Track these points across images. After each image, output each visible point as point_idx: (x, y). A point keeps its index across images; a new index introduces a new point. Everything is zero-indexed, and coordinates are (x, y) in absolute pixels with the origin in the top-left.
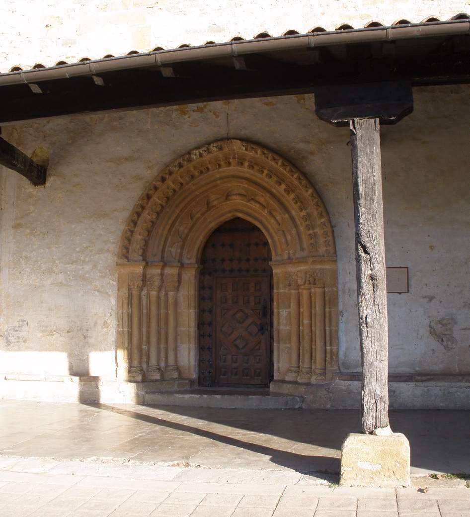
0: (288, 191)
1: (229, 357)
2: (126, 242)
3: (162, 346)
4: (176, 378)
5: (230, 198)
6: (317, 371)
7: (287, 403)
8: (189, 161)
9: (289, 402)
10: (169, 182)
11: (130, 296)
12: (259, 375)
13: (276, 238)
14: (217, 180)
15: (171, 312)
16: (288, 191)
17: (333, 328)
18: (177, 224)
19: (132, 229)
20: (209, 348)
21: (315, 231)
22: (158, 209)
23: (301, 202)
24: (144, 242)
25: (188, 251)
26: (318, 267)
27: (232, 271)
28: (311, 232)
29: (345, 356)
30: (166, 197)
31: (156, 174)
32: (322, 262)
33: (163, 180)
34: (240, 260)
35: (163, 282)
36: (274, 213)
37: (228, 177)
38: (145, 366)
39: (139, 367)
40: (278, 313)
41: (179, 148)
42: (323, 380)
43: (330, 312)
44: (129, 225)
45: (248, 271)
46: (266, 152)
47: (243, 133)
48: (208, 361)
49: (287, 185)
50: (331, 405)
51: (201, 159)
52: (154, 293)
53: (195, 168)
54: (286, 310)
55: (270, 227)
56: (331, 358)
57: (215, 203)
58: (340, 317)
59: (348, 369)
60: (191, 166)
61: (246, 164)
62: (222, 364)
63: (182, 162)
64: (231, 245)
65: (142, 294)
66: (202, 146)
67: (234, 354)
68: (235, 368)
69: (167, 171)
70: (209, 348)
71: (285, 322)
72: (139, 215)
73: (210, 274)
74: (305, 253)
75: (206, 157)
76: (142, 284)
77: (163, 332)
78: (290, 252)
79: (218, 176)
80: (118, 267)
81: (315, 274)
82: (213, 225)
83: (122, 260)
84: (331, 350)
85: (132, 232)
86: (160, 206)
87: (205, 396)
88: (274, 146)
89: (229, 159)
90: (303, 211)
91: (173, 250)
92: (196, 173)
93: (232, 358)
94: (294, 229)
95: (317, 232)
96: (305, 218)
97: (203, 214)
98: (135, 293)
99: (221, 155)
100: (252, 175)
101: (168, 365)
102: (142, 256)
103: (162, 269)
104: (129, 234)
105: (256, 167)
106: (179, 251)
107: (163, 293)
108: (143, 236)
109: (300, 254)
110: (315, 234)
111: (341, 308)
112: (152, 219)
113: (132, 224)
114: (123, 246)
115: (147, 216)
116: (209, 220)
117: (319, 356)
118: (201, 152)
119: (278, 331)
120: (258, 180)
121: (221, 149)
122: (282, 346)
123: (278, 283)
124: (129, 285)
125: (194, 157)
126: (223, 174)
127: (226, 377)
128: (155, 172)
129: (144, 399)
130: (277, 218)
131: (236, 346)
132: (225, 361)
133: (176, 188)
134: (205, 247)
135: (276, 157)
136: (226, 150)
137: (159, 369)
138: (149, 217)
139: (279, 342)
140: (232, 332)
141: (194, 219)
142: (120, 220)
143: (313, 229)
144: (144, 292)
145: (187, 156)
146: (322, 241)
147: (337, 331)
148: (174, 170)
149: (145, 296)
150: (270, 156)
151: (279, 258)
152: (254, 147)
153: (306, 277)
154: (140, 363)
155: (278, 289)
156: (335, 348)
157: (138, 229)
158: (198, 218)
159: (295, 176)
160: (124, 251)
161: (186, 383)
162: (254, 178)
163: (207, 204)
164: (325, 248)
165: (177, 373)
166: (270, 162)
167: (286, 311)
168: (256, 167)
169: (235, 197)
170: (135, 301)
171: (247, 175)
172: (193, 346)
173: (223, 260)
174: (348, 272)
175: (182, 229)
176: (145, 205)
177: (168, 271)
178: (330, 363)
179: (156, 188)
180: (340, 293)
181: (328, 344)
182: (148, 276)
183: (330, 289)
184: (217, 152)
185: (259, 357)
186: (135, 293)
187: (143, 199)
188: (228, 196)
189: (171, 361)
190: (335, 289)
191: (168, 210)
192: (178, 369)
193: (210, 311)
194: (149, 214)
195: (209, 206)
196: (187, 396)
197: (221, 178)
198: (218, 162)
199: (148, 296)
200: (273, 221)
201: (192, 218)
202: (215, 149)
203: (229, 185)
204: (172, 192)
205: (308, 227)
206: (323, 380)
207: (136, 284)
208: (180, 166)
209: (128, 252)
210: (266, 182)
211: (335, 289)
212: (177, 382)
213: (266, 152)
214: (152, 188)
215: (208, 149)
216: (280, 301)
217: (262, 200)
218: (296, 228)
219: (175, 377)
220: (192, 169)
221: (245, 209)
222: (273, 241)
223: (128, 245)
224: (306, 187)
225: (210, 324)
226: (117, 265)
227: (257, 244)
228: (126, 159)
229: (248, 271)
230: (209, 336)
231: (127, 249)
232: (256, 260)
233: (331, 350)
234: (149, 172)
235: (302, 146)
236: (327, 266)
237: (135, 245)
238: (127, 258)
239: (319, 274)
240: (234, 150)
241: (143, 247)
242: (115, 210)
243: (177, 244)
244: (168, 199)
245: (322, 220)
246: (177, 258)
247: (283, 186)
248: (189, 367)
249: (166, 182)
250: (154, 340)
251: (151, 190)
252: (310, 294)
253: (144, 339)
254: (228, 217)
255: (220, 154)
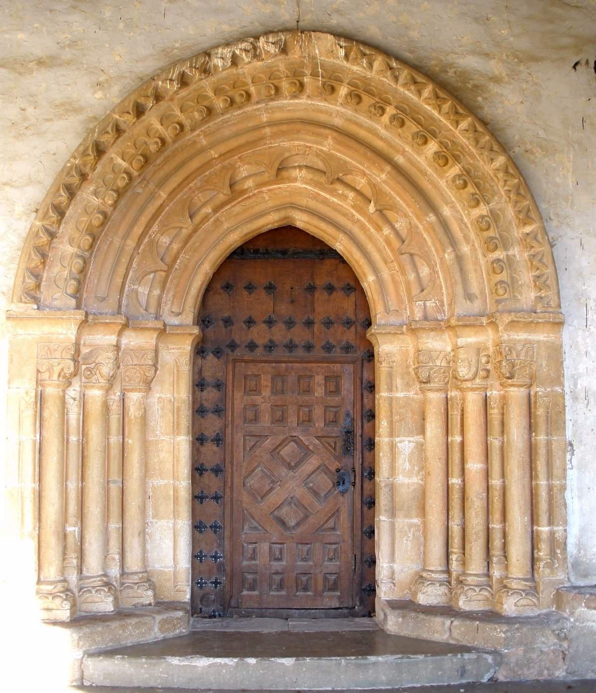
0: (444, 158)
1: (265, 547)
2: (36, 260)
3: (114, 525)
4: (150, 605)
5: (285, 174)
6: (514, 585)
7: (463, 672)
8: (206, 71)
9: (469, 667)
10: (152, 119)
11: (41, 400)
12: (334, 587)
13: (386, 274)
14: (264, 127)
15: (133, 441)
16: (444, 158)
17: (556, 482)
18: (155, 228)
19: (53, 229)
20: (215, 527)
21: (510, 253)
22: (121, 183)
23: (477, 185)
24: (80, 261)
25: (174, 296)
26: (522, 336)
27: (270, 347)
28: (499, 254)
29: (580, 546)
30: (142, 155)
31: (117, 101)
32: (530, 326)
33: (139, 111)
34: (290, 323)
35: (118, 367)
36: (390, 214)
37: (290, 121)
38: (73, 577)
39: (60, 581)
40: (393, 447)
41: (177, 45)
42: (535, 605)
43: (549, 444)
44: (45, 216)
45: (309, 347)
46: (394, 65)
47: (335, 21)
48: (212, 557)
49: (441, 143)
50: (566, 670)
51: (234, 71)
52: (96, 394)
53: (217, 91)
54: (412, 439)
55: (370, 247)
56: (552, 553)
57: (249, 183)
58: (568, 457)
59: (585, 576)
60: (207, 85)
61: (343, 91)
62: (245, 563)
63: (188, 71)
64: (270, 288)
65: (67, 397)
66: (241, 40)
67: (274, 539)
68: (277, 573)
69: (150, 91)
70: (215, 527)
71: (407, 466)
72: (71, 192)
73: (218, 353)
74: (476, 306)
75: (249, 67)
76: (72, 369)
77: (114, 490)
78: (428, 304)
79: (265, 118)
80: (10, 323)
81: (514, 353)
82: (235, 239)
83: (22, 305)
84: (552, 534)
85: (52, 235)
86: (125, 176)
87: (252, 661)
88: (408, 55)
89: (303, 75)
90: (482, 204)
91: (143, 290)
92: (219, 104)
93: (270, 548)
94: (450, 250)
95: (514, 256)
96: (487, 221)
97: (216, 210)
98: (51, 391)
99: (282, 67)
100: (349, 120)
101: (126, 570)
102: (74, 296)
103: (120, 334)
104: (45, 238)
105: (367, 100)
106: (157, 292)
107: (116, 395)
108: (79, 247)
109: (463, 307)
110: (510, 260)
111: (569, 434)
112: (102, 207)
113: (54, 216)
114: (28, 269)
115: (88, 196)
116: (226, 226)
117: (518, 550)
118: (238, 52)
119: (392, 487)
120: (362, 134)
121: (284, 50)
122: (401, 521)
123: (390, 375)
124: (38, 371)
125: (220, 63)
126: (278, 115)
127: (256, 593)
128: (114, 95)
129: (83, 675)
130: (397, 226)
131: (282, 522)
132: (253, 558)
133: (168, 134)
134: (208, 290)
135: (420, 79)
136: (295, 55)
137: (107, 584)
138: (96, 201)
139: (393, 513)
140: (272, 489)
141: (198, 219)
142: (19, 208)
143: (506, 248)
144: (73, 392)
145: (202, 60)
146: (526, 277)
147: (563, 488)
148: (166, 90)
149: (74, 399)
150: (405, 74)
151: (393, 319)
152: (368, 52)
153: (478, 361)
154: (63, 570)
155: (390, 389)
156: (559, 529)
157: (67, 229)
158: (206, 218)
159: (464, 124)
160: (31, 282)
161: (178, 619)
162: (353, 129)
163: (231, 186)
164: (533, 295)
165: (150, 593)
166: (402, 89)
167: (410, 442)
168: (367, 100)
169: (296, 173)
170: (52, 412)
171: (338, 122)
172: (184, 525)
173: (250, 322)
174: (583, 350)
175: (165, 240)
176: (87, 170)
177: (131, 340)
178: (550, 566)
179: (119, 130)
180: (568, 402)
181: (543, 517)
182: (85, 351)
183: (549, 389)
184: (275, 56)
185: (334, 547)
186: (51, 391)
187: (85, 154)
188: (281, 170)
189: (134, 563)
190: (558, 389)
191: (140, 190)
192: (148, 580)
193: (218, 440)
194: (96, 193)
195: (235, 191)
196: (202, 662)
197: (271, 124)
198: (274, 82)
199: (83, 402)
200: (387, 231)
201: (191, 217)
202: (272, 49)
203: (286, 144)
204: (157, 143)
205: (491, 245)
206: (535, 605)
207: (57, 370)
208: (183, 81)
209: (38, 286)
210: (381, 139)
211: (558, 389)
212: (159, 618)
213: (394, 65)
214: (109, 129)
215: (255, 48)
216: (396, 418)
217: (361, 183)
218: (452, 246)
219: (148, 602)
220: (211, 94)
221: (312, 204)
222: (380, 281)
223: (41, 267)
224: (491, 150)
225: (217, 471)
226: (8, 318)
227: (330, 289)
228: (41, 63)
229: (309, 347)
230: (216, 498)
231: (38, 277)
232: (328, 323)
233: (552, 534)
234: (99, 95)
235: (470, 62)
236: (541, 336)
237: (56, 269)
238: (36, 300)
239: (523, 354)
240: (314, 58)
241: (77, 276)
242: (5, 184)
243: (152, 276)
244: (147, 160)
245: (528, 229)
246: (152, 310)
247: (433, 147)
248: (175, 574)
249: (143, 118)
250: (94, 509)
251: (108, 133)
252: (486, 401)
253: (73, 508)
254: (271, 221)
255: (281, 65)
